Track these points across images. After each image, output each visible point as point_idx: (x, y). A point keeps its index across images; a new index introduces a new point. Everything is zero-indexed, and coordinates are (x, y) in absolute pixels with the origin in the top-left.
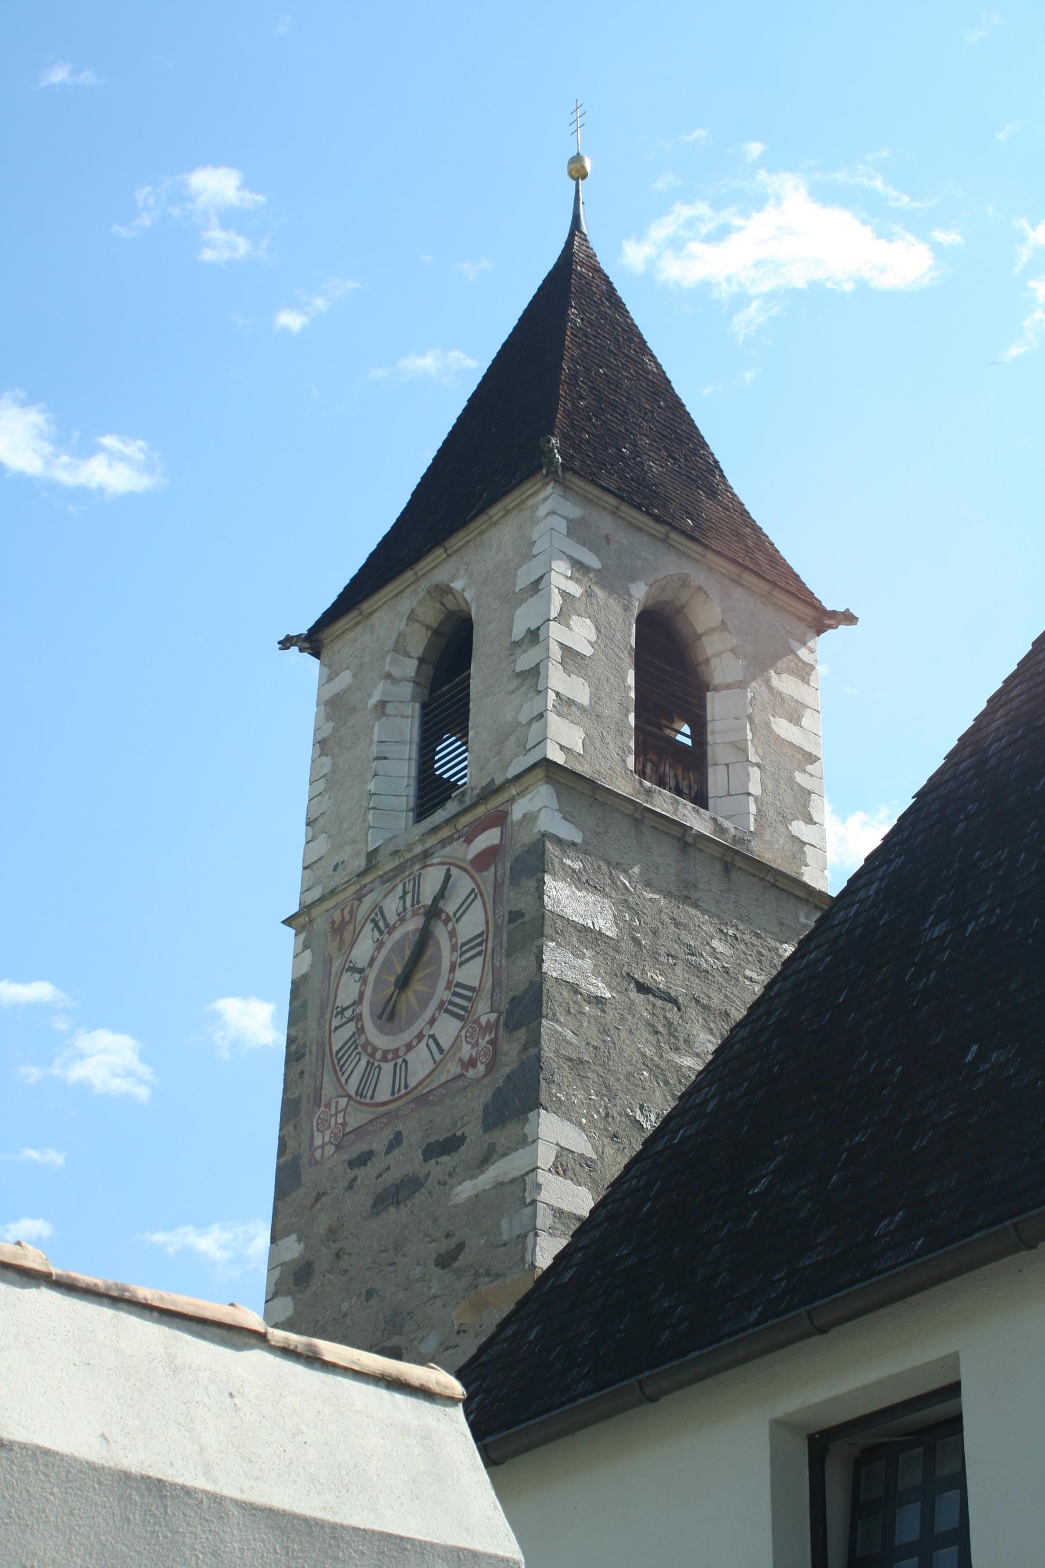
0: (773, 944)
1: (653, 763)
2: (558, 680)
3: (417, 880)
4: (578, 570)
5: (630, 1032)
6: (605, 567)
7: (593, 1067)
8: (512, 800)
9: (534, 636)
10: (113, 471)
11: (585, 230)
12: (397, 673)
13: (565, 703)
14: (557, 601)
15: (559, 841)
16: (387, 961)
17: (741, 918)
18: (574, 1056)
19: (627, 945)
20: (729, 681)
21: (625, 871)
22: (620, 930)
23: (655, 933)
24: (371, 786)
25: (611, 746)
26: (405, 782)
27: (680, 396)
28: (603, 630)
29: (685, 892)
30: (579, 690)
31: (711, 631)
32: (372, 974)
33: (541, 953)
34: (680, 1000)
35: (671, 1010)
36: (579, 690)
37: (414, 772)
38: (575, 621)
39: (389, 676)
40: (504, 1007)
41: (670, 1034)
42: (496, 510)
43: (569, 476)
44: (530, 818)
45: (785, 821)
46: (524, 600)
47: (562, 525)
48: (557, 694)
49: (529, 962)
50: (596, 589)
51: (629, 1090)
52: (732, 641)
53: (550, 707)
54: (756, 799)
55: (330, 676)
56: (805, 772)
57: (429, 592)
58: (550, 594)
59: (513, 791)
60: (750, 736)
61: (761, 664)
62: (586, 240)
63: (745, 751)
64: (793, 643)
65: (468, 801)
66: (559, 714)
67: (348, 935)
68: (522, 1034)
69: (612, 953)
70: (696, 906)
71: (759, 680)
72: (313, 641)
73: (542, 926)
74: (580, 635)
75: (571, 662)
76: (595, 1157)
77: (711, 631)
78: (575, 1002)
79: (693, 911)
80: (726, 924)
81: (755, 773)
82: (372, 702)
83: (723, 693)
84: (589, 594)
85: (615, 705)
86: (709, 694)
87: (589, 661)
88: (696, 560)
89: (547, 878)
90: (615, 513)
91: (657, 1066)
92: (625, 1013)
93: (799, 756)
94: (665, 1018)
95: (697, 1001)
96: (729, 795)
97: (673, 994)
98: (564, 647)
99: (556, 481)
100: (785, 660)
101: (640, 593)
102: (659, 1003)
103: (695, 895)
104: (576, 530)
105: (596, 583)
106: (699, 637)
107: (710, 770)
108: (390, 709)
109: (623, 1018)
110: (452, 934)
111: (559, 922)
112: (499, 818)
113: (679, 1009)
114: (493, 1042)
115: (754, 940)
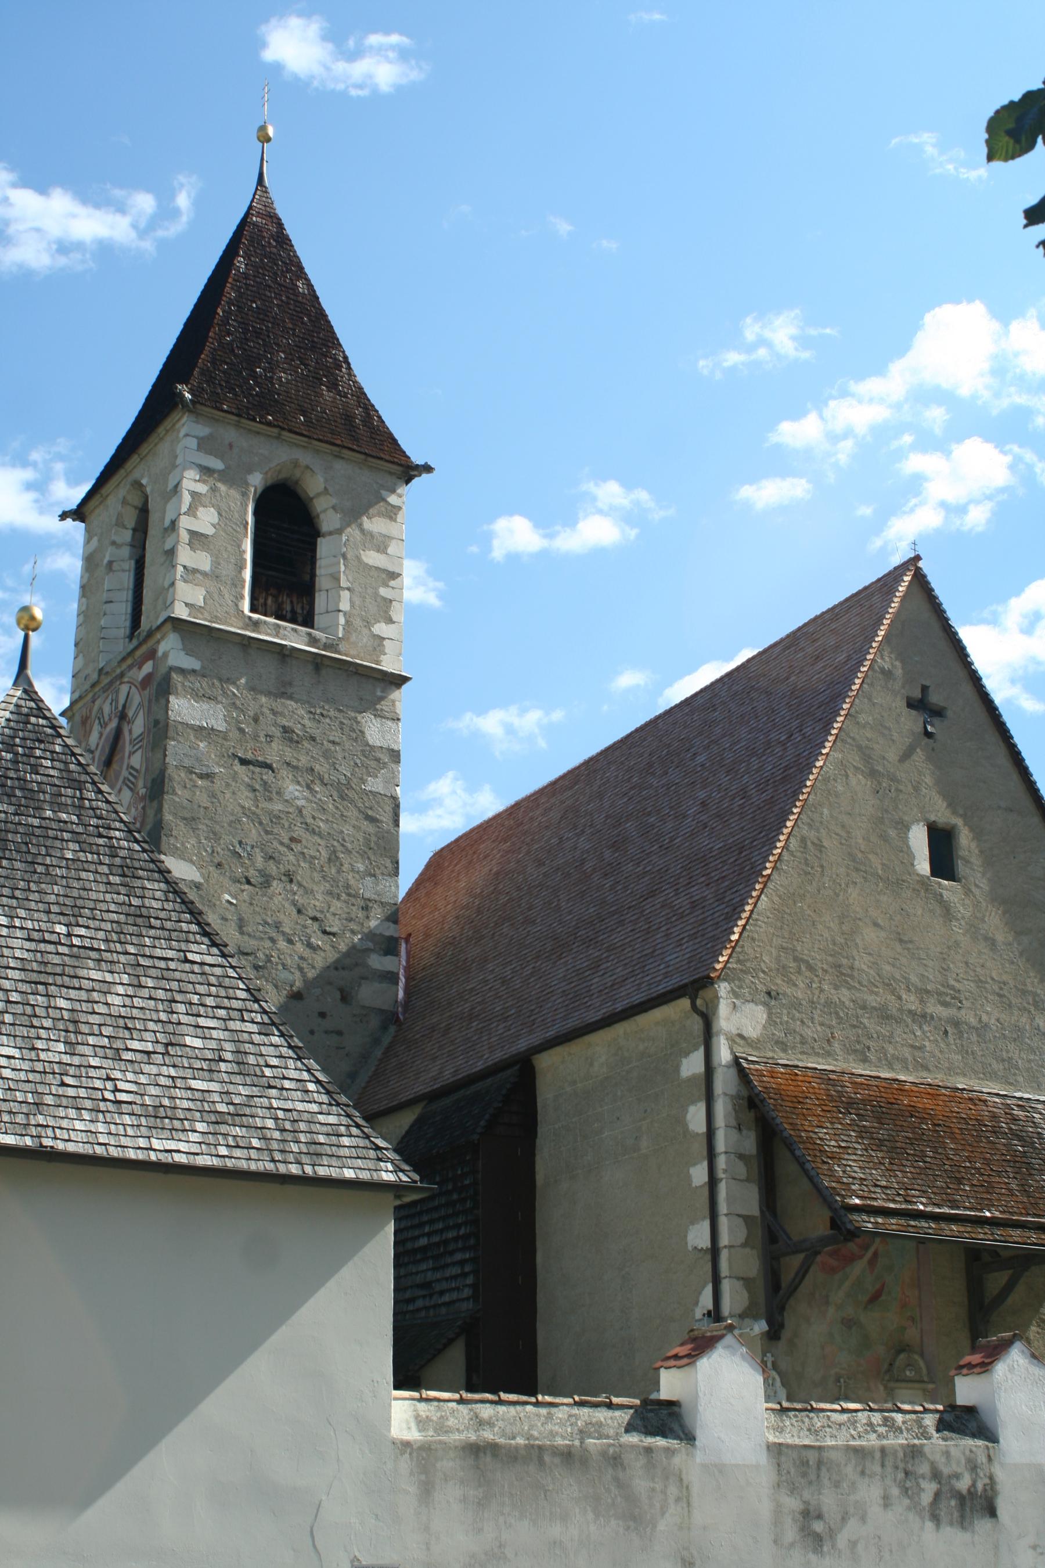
0: (353, 714)
1: (273, 596)
2: (185, 556)
3: (117, 692)
4: (205, 474)
5: (234, 793)
6: (228, 467)
7: (203, 821)
8: (158, 642)
9: (174, 525)
10: (380, 69)
11: (267, 183)
12: (119, 540)
13: (191, 572)
14: (187, 499)
15: (182, 671)
16: (103, 746)
17: (327, 701)
18: (188, 816)
19: (234, 734)
20: (331, 529)
21: (234, 683)
22: (229, 724)
23: (256, 720)
24: (102, 623)
25: (227, 596)
26: (123, 617)
27: (115, 448)
28: (224, 514)
29: (283, 690)
30: (202, 561)
31: (318, 495)
32: (97, 754)
33: (165, 750)
34: (274, 765)
35: (267, 773)
36: (202, 561)
37: (129, 610)
38: (201, 512)
39: (114, 543)
40: (149, 785)
41: (265, 790)
42: (161, 430)
43: (198, 406)
44: (166, 655)
45: (368, 625)
46: (170, 498)
47: (193, 443)
48: (185, 567)
49: (160, 755)
50: (219, 485)
51: (231, 833)
52: (333, 501)
53: (178, 577)
54: (345, 614)
55: (89, 534)
56: (388, 586)
57: (132, 485)
58: (181, 496)
59: (158, 636)
60: (342, 568)
61: (354, 514)
62: (266, 192)
63: (338, 580)
64: (384, 493)
65: (141, 639)
66: (185, 581)
67: (88, 726)
68: (155, 804)
69: (220, 741)
70: (291, 698)
71: (353, 526)
72: (79, 513)
73: (167, 731)
74: (206, 520)
75: (196, 542)
76: (202, 881)
77: (318, 495)
78: (191, 780)
79: (289, 702)
80: (315, 707)
81: (345, 595)
82: (105, 561)
83: (328, 538)
84: (214, 490)
85: (231, 567)
86: (319, 539)
87: (210, 539)
88: (304, 447)
89: (172, 698)
90: (237, 425)
91: (254, 813)
92: (230, 781)
93: (384, 576)
94: (262, 779)
95: (288, 764)
96: (327, 612)
97: (268, 762)
98: (193, 534)
99: (190, 411)
100: (377, 507)
101: (257, 481)
102: (258, 770)
103: (290, 691)
104: (204, 445)
105: (219, 480)
106: (311, 499)
107: (317, 595)
108: (115, 566)
109: (228, 785)
110: (130, 731)
111: (180, 727)
112: (152, 654)
113: (273, 772)
114: (144, 808)
115: (337, 714)
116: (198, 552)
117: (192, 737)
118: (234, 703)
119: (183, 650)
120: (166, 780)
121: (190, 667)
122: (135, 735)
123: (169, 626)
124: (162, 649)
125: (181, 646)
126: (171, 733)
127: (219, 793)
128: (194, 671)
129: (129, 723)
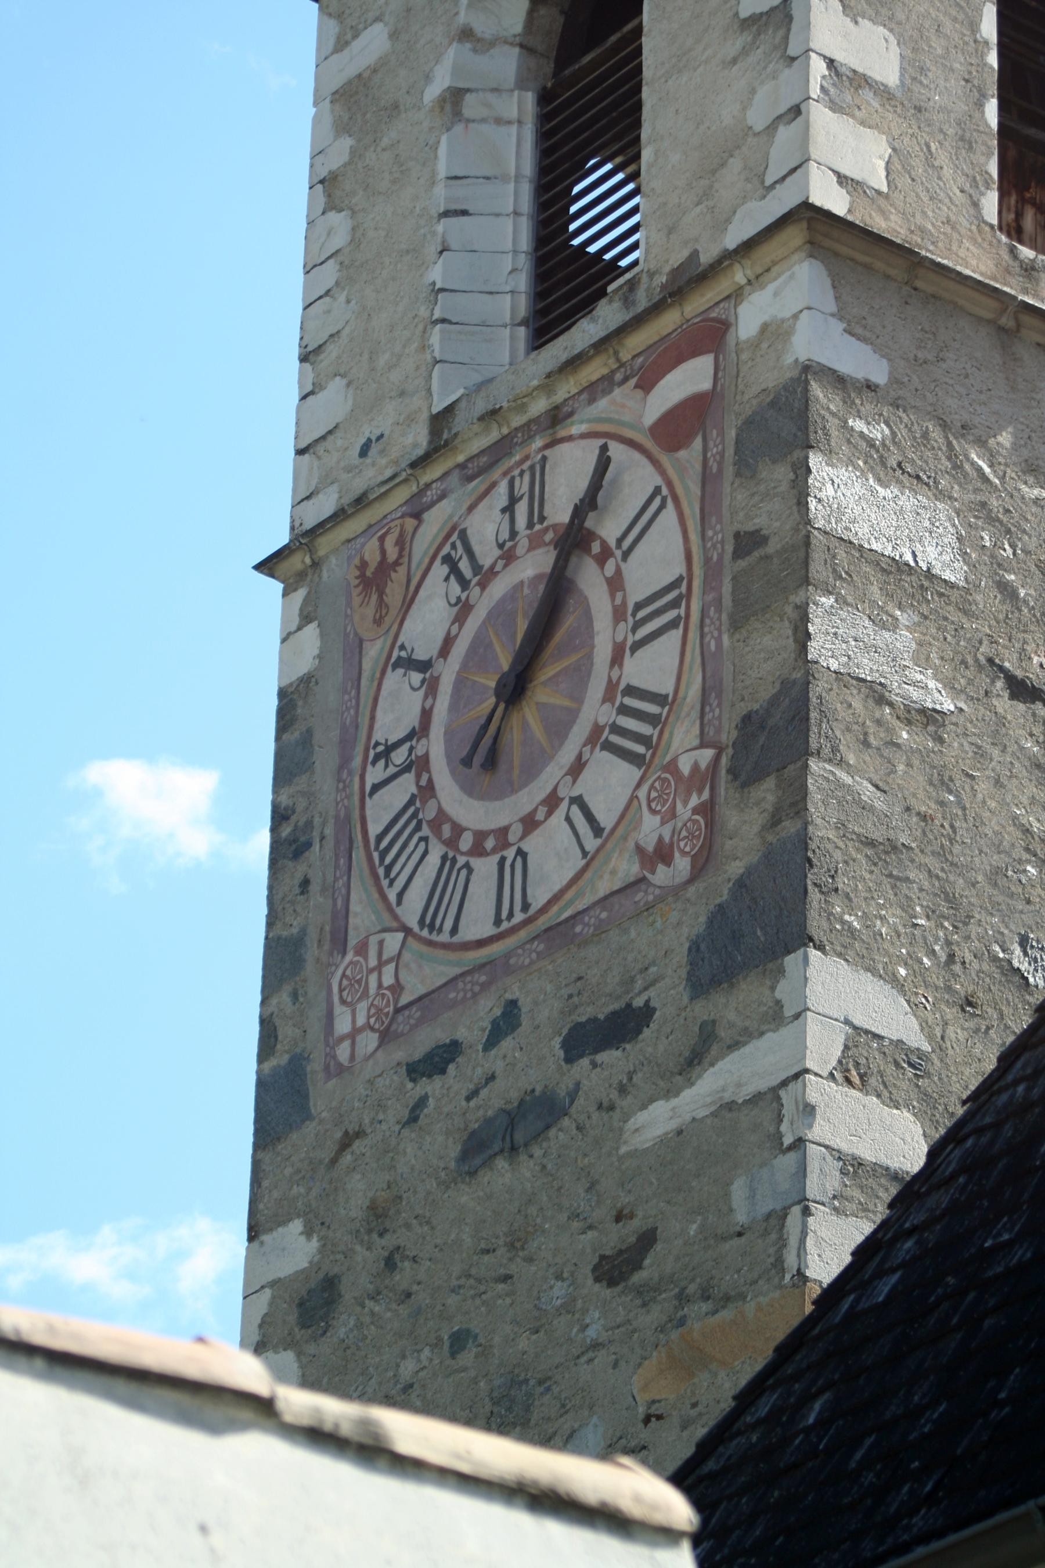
3: (539, 472)
5: (998, 783)
8: (737, 295)
12: (483, 26)
15: (839, 381)
18: (878, 835)
19: (987, 600)
21: (981, 443)
24: (436, 274)
25: (947, 172)
26: (507, 263)
32: (448, 673)
37: (525, 242)
39: (466, 34)
40: (728, 735)
44: (775, 332)
48: (831, 63)
53: (815, 91)
59: (739, 276)
65: (642, 300)
66: (835, 107)
67: (394, 593)
68: (767, 792)
69: (955, 616)
76: (926, 1047)
78: (879, 722)
82: (433, 92)
85: (955, 85)
92: (986, 744)
108: (471, 106)
109: (980, 754)
110: (615, 584)
111: (841, 553)
112: (711, 336)
114: (707, 810)
116: (865, 23)
117: (875, 590)
118: (984, 505)
119: (839, 315)
120: (814, 715)
121: (860, 374)
122: (637, 589)
123: (795, 235)
124: (749, 319)
125: (833, 308)
126: (818, 569)
127: (958, 776)
128: (870, 386)
129: (602, 559)
